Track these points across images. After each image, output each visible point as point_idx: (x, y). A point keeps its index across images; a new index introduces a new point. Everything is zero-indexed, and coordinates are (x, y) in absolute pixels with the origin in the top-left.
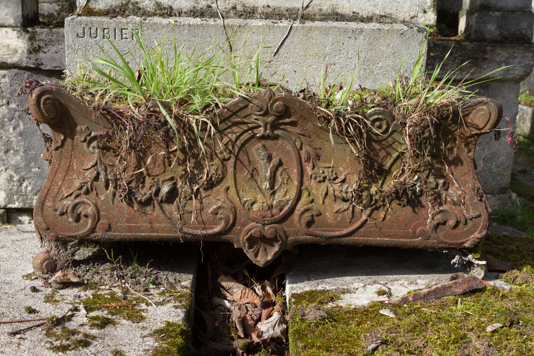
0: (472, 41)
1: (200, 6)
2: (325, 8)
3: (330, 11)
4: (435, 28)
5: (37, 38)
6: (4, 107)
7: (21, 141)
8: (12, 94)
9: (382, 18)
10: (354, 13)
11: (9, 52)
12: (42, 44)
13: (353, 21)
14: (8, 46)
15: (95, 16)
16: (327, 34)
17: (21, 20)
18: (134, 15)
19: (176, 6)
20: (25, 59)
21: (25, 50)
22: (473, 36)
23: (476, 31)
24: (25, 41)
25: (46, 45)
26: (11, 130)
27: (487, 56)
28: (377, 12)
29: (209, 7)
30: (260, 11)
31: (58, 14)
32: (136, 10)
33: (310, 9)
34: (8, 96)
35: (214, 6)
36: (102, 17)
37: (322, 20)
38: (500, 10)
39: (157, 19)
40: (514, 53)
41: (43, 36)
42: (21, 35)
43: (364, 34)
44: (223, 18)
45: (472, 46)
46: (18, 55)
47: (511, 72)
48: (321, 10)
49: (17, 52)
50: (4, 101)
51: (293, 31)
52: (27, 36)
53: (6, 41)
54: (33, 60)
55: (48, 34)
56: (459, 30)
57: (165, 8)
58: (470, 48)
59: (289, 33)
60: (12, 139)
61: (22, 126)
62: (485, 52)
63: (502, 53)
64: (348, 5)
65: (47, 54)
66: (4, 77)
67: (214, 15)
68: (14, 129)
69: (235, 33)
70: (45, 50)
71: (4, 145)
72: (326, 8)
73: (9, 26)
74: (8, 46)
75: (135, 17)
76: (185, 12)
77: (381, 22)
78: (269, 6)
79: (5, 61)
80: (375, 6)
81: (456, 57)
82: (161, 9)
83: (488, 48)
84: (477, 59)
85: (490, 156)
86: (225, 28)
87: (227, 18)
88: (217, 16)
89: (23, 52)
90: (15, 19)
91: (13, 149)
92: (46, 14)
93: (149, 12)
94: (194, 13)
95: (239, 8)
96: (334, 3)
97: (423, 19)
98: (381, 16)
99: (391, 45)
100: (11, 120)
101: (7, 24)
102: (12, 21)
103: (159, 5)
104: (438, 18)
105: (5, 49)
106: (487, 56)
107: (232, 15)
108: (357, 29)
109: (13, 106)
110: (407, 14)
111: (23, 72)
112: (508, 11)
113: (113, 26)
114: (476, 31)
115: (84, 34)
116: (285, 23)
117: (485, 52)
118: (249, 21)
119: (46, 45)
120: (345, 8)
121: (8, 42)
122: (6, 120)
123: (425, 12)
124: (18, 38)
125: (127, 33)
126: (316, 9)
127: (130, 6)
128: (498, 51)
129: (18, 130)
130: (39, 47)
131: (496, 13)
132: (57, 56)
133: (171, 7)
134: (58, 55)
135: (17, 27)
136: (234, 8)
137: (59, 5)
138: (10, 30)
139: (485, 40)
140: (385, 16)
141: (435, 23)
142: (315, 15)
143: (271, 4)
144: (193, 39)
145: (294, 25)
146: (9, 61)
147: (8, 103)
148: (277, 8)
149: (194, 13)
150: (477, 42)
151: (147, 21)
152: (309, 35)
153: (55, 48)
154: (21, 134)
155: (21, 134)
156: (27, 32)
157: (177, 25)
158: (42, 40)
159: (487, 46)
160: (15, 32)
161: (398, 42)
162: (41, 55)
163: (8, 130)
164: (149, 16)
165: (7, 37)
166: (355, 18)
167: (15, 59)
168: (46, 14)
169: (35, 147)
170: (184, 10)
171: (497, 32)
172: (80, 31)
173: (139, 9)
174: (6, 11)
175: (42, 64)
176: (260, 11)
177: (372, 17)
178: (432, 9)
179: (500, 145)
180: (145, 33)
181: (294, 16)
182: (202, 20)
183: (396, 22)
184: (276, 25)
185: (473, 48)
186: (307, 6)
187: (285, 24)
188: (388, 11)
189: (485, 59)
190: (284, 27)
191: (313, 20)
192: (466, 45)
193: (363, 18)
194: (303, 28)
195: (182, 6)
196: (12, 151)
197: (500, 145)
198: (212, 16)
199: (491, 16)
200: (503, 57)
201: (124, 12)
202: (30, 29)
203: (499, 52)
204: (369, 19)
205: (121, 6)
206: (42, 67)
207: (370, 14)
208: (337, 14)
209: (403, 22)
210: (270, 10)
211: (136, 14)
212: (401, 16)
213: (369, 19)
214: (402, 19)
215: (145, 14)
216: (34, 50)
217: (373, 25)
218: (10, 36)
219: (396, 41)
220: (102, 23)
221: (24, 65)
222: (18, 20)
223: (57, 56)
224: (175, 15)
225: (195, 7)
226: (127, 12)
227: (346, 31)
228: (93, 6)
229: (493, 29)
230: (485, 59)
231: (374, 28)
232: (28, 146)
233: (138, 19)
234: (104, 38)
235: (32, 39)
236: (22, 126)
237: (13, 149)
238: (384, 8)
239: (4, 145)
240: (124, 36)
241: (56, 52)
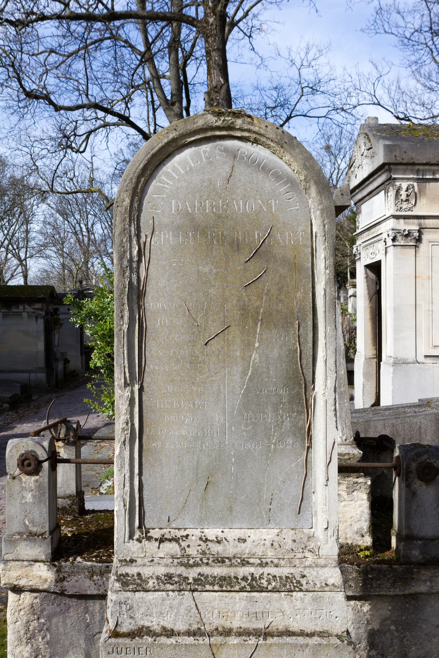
0: (401, 564)
1: (193, 628)
2: (280, 628)
3: (284, 629)
4: (371, 550)
5: (63, 570)
6: (35, 621)
7: (48, 648)
8: (42, 611)
9: (322, 634)
10: (301, 630)
11: (41, 581)
12: (66, 575)
13: (301, 636)
14: (41, 577)
15: (120, 637)
16: (282, 648)
17: (51, 557)
18: (147, 635)
19: (176, 629)
20: (53, 586)
21: (53, 580)
22: (402, 560)
23: (403, 556)
24: (53, 573)
25: (69, 576)
26: (40, 639)
27: (414, 576)
28: (318, 630)
29: (199, 629)
30: (235, 631)
31: (70, 507)
32: (149, 632)
33: (270, 628)
34: (39, 613)
35: (202, 628)
36: (125, 639)
37: (278, 636)
38: (421, 539)
39: (163, 640)
40: (436, 572)
41: (67, 569)
42: (51, 568)
43: (309, 647)
44: (209, 636)
45: (402, 569)
46: (48, 583)
47: (435, 588)
48: (277, 629)
49: (47, 581)
50: (36, 616)
51: (258, 647)
52: (55, 569)
53: (38, 573)
54: (59, 588)
55: (71, 568)
56: (392, 546)
57: (169, 631)
58: (400, 570)
59: (256, 649)
60: (40, 647)
61: (48, 637)
62: (412, 573)
63: (426, 574)
64: (297, 625)
65: (70, 583)
66: (36, 598)
67: (202, 634)
68: (43, 638)
69: (218, 649)
70: (68, 580)
71: (34, 652)
72: (281, 628)
73: (42, 561)
74: (41, 577)
75: (148, 637)
76: (183, 633)
77: (321, 636)
78: (241, 628)
79: (37, 588)
80: (316, 625)
81: (389, 578)
82: (166, 631)
83: (415, 570)
84: (406, 579)
85: (424, 654)
86: (210, 646)
87: (212, 636)
88: (205, 635)
89: (52, 581)
90: (46, 556)
91: (41, 655)
92: (60, 507)
93: (157, 633)
94: (189, 633)
95: (220, 629)
96: (287, 624)
97: (362, 541)
98: (321, 632)
99: (329, 655)
100: (40, 631)
101: (40, 560)
102: (43, 557)
103: (164, 628)
104: (373, 541)
105: (38, 579)
106: (414, 576)
107: (215, 634)
108: (304, 644)
109: (42, 620)
110: (339, 630)
111: (51, 594)
112: (428, 539)
113: (133, 646)
114: (403, 556)
115: (113, 652)
116: (252, 641)
117: (412, 573)
118: (227, 638)
119: (69, 576)
120: (295, 627)
121: (40, 573)
122: (37, 631)
123: (363, 536)
124: (48, 570)
125: (142, 651)
126: (274, 629)
127: (144, 629)
128: (423, 572)
129: (46, 639)
130: (64, 577)
131: (419, 542)
132: (77, 584)
133: (172, 630)
134: (78, 583)
135: (47, 562)
136: (217, 629)
137: (70, 500)
138: (41, 564)
139: (412, 564)
140: (324, 632)
141: (371, 545)
142: (274, 632)
143: (242, 626)
144: (189, 654)
145: (259, 642)
146: (41, 588)
147: (38, 619)
148: (246, 628)
149: (189, 633)
150: (406, 565)
151: (156, 642)
152: (270, 649)
153: (76, 578)
154: (48, 643)
155: (48, 643)
156: (55, 566)
157: (177, 646)
158: (66, 572)
159: (414, 568)
160: (46, 566)
161: (333, 652)
162: (65, 583)
163: (38, 640)
164: (158, 636)
165: (40, 570)
166: (302, 634)
167: (45, 586)
168: (60, 507)
169: (58, 653)
170: (182, 632)
171: (421, 557)
172: (111, 650)
173: (151, 631)
174: (40, 549)
175: (66, 590)
176: (235, 631)
177: (314, 633)
178: (368, 534)
179: (432, 645)
180: (155, 650)
181: (259, 633)
182: (195, 640)
183: (332, 636)
184: (246, 643)
185: (402, 570)
186: (268, 627)
187: (253, 642)
188: (325, 628)
189: (413, 579)
190: (252, 644)
191: (272, 636)
192: (396, 568)
193: (308, 634)
194: (266, 644)
195: (180, 629)
196: (40, 656)
197: (432, 645)
198: (201, 636)
199: (415, 544)
200: (427, 576)
201: (140, 633)
202: (56, 563)
203: (424, 573)
204: (311, 635)
205: (138, 630)
206: (66, 593)
207: (312, 631)
208: (289, 631)
209: (337, 636)
210: (242, 630)
211: (148, 635)
212: (335, 632)
213: (311, 635)
214: (336, 634)
215: (154, 634)
216: (60, 580)
217: (316, 640)
218: (42, 570)
219: (333, 652)
220: (125, 644)
221: (52, 590)
222: (48, 556)
223: (77, 584)
224: (176, 635)
225: (189, 629)
226: (142, 634)
227: (296, 645)
228: (119, 630)
229: (417, 554)
230: (413, 579)
231: (316, 643)
232: (53, 653)
233: (150, 640)
234: (127, 654)
235: (59, 571)
236: (48, 637)
237: (41, 655)
238: (322, 627)
239: (34, 652)
240: (141, 653)
241: (77, 581)
